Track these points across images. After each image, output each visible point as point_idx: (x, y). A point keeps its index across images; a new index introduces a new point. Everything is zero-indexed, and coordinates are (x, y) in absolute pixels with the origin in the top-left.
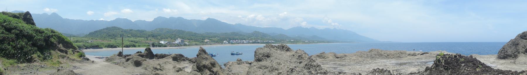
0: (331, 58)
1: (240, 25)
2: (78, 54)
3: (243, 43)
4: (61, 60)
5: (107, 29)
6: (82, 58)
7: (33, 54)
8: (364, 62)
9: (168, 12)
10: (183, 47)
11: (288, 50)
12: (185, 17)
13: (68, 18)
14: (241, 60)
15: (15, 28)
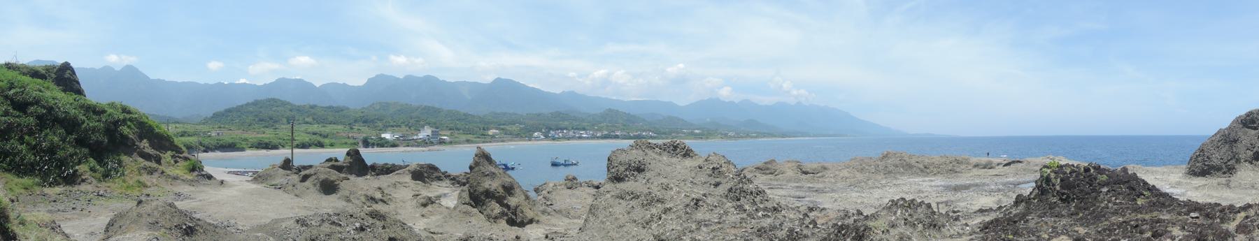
0: (790, 173)
1: (572, 94)
3: (580, 138)
4: (145, 178)
5: (256, 103)
7: (79, 163)
8: (870, 183)
9: (401, 64)
10: (436, 147)
11: (688, 153)
12: (442, 76)
14: (574, 178)
15: (37, 102)
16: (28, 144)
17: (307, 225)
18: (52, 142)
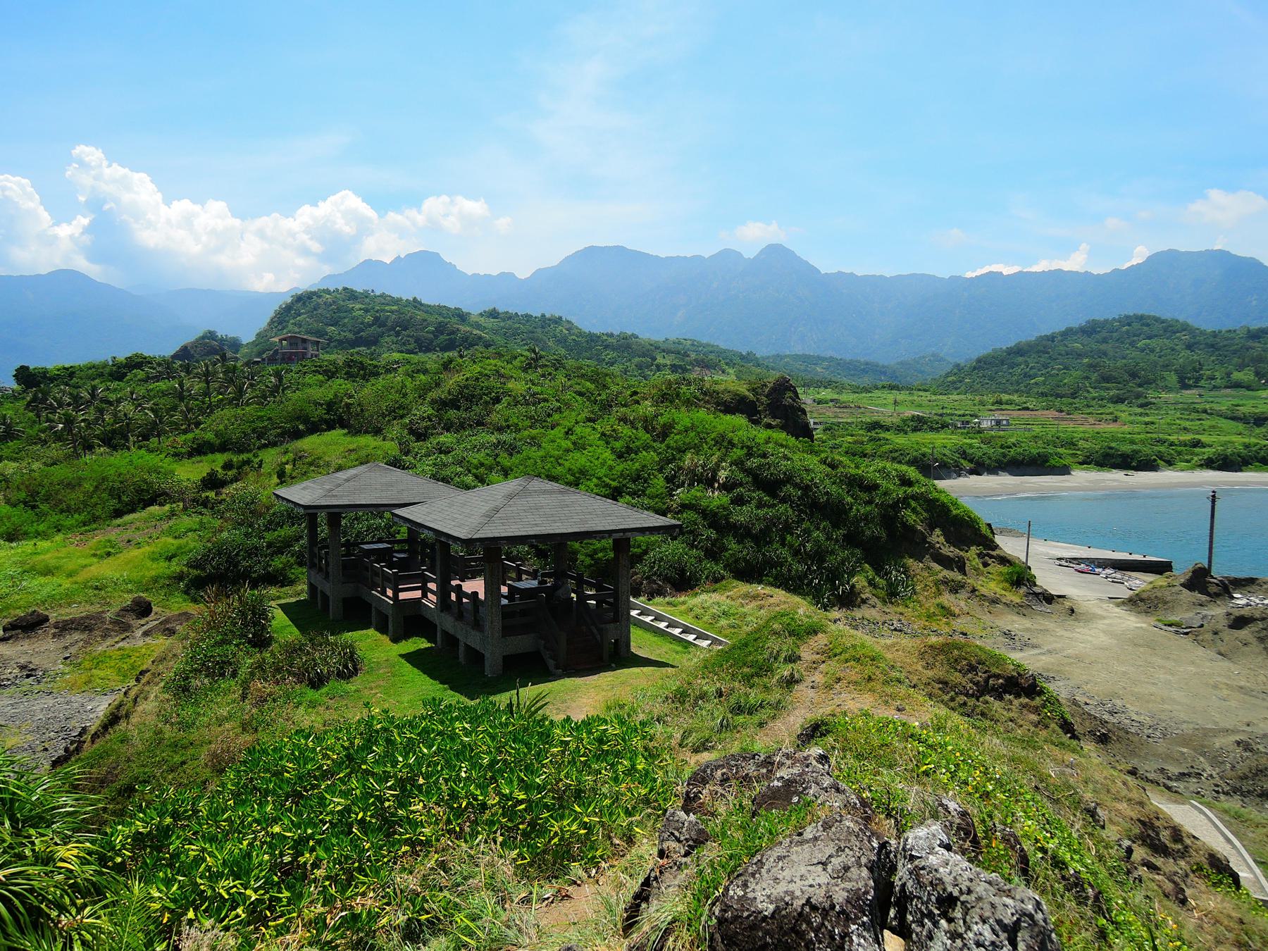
2: (1005, 569)
4: (947, 599)
5: (1091, 330)
6: (1023, 590)
7: (852, 574)
13: (847, 270)
15: (789, 479)
16: (791, 546)
17: (1251, 750)
18: (817, 541)
